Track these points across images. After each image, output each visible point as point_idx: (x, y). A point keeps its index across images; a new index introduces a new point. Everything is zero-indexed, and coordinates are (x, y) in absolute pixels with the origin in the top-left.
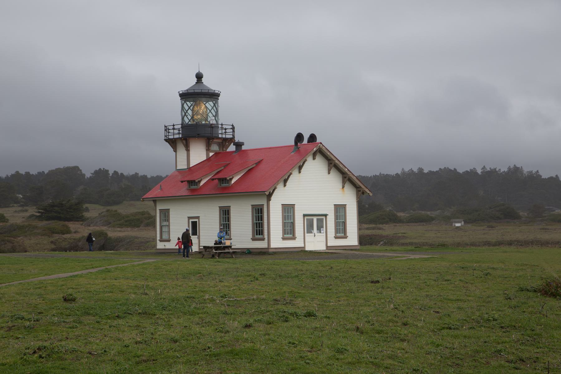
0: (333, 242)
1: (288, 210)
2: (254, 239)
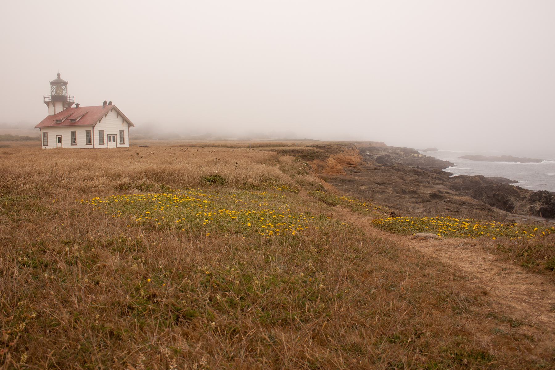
0: (119, 146)
1: (101, 133)
2: (87, 144)
